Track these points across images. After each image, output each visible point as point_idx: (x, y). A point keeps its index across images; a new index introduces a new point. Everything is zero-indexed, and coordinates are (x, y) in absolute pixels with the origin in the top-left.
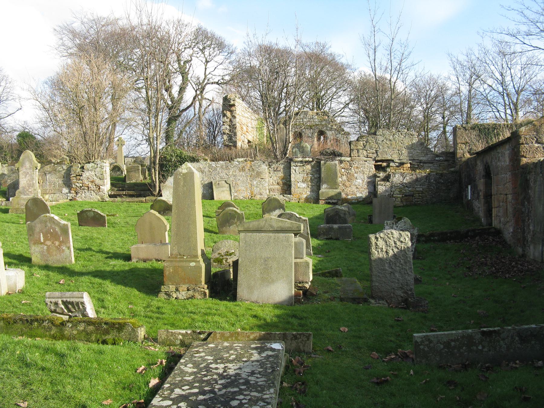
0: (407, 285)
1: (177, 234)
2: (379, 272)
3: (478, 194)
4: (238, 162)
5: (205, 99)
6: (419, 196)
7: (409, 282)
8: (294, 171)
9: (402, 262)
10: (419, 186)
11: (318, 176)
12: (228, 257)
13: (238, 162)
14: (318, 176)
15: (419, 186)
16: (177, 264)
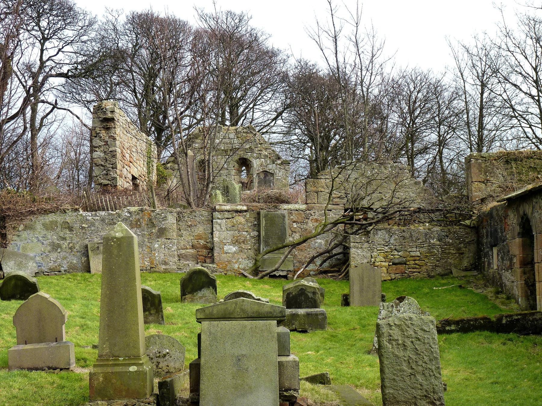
0: (434, 392)
1: (108, 326)
2: (394, 374)
3: (511, 260)
4: (130, 213)
5: (43, 102)
6: (416, 264)
7: (436, 388)
8: (218, 228)
9: (426, 359)
10: (414, 249)
11: (256, 233)
12: (159, 360)
13: (130, 213)
14: (256, 233)
15: (414, 249)
16: (109, 370)
